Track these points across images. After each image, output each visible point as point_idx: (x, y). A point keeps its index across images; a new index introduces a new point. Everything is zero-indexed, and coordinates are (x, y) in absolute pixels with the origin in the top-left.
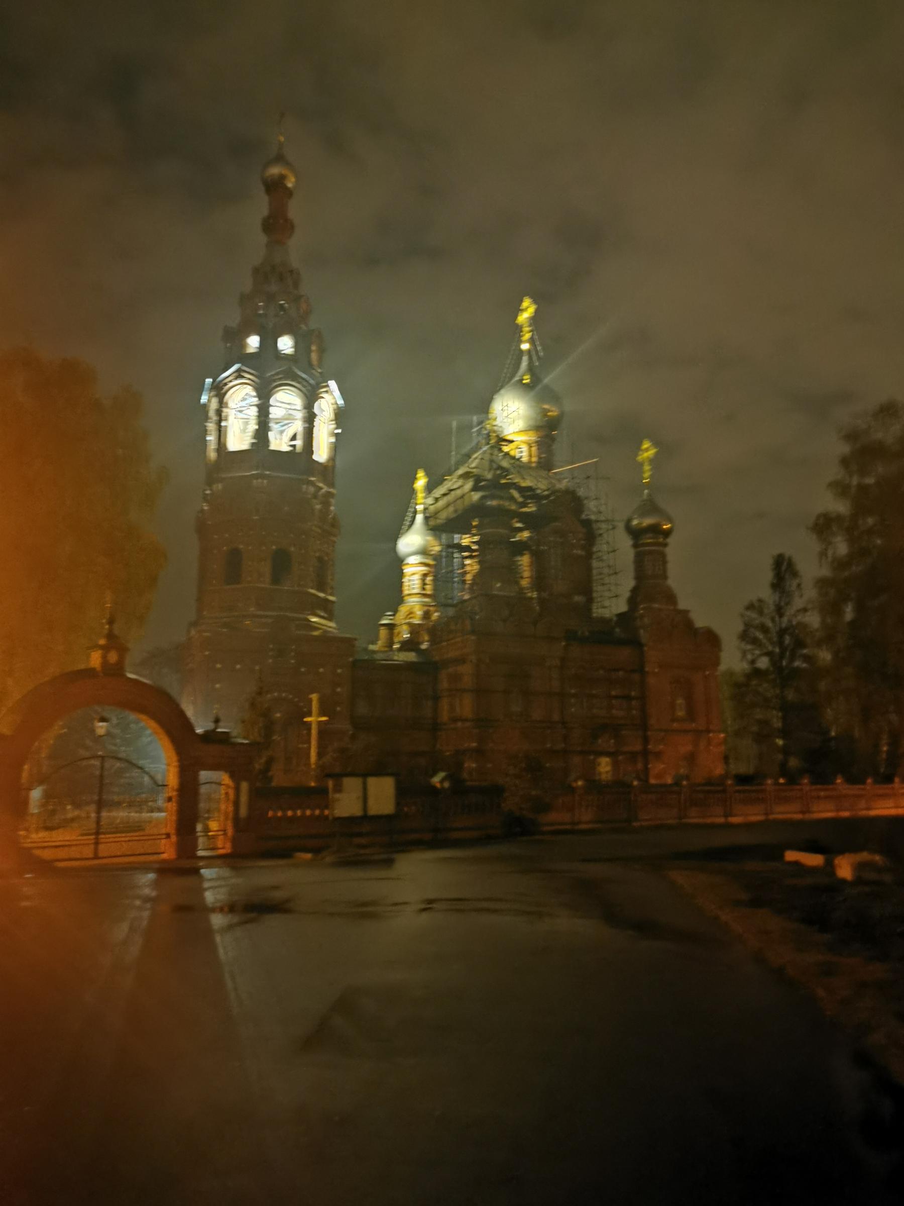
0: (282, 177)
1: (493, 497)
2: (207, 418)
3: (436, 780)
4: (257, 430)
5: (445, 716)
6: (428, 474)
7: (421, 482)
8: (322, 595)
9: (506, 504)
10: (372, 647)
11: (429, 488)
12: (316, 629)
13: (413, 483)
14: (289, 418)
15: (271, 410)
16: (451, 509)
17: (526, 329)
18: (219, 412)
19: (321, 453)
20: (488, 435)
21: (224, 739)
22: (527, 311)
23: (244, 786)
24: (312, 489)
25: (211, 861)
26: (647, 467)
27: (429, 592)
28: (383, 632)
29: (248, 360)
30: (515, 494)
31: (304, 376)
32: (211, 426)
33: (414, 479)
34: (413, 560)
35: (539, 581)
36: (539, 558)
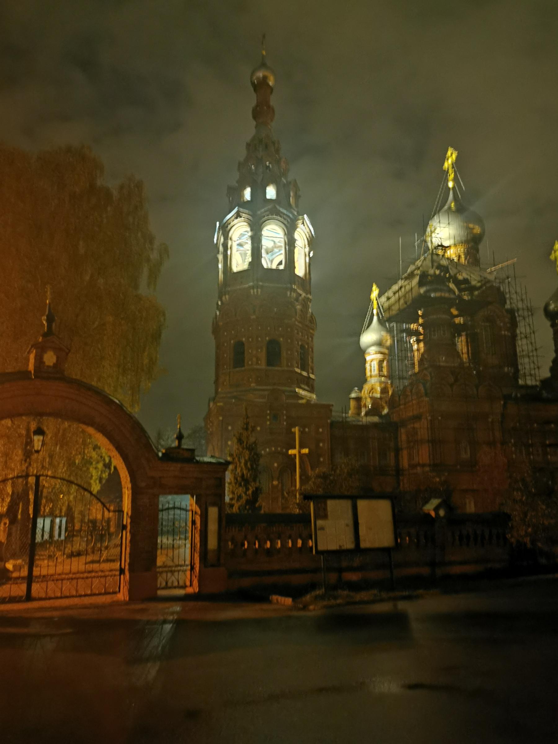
0: (265, 78)
1: (435, 290)
3: (430, 507)
5: (405, 463)
6: (378, 286)
8: (305, 374)
12: (302, 398)
13: (370, 294)
16: (402, 301)
17: (450, 171)
18: (225, 246)
19: (300, 270)
22: (452, 156)
24: (294, 295)
28: (352, 404)
30: (452, 286)
31: (285, 212)
32: (220, 257)
33: (370, 291)
34: (373, 350)
35: (475, 354)
36: (473, 340)
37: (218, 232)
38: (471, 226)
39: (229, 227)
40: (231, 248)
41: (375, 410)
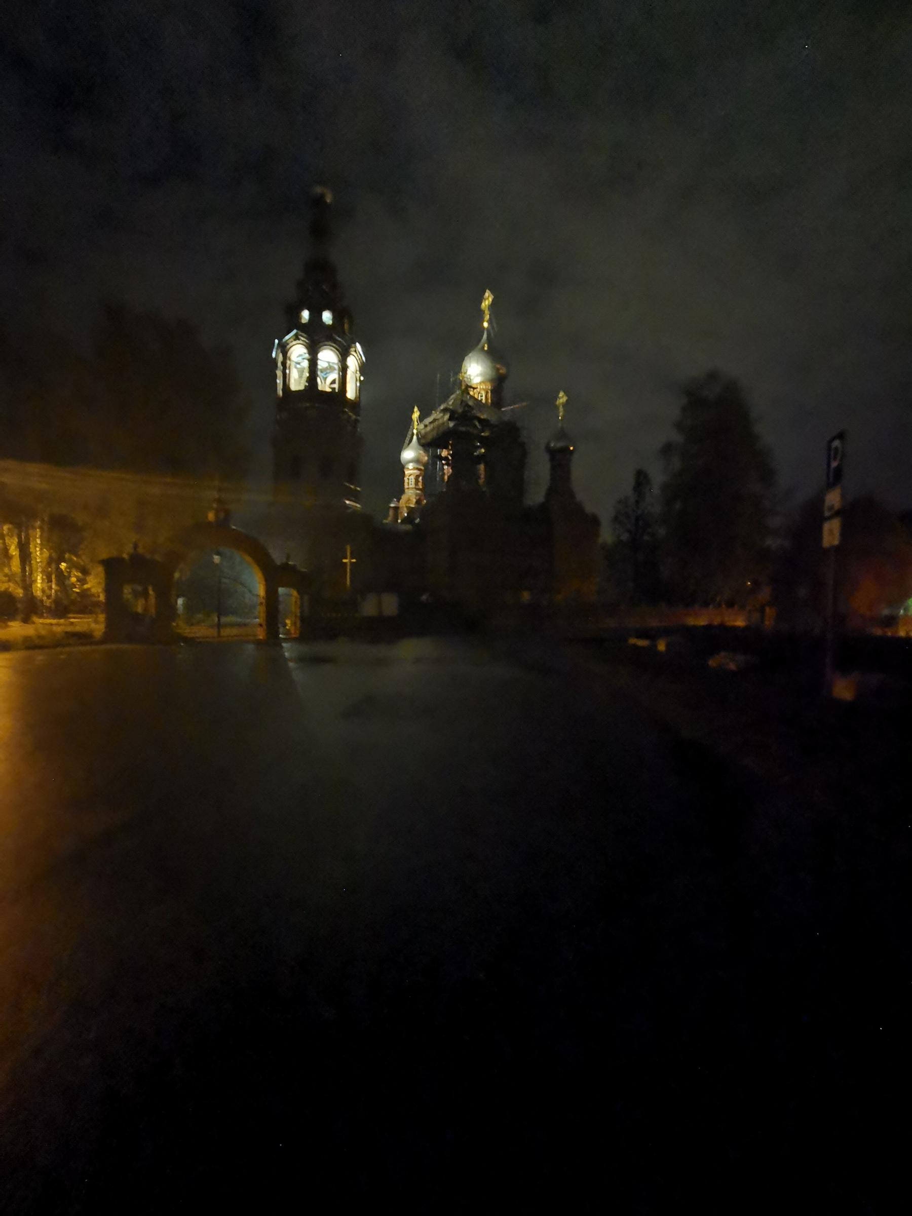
2: (276, 367)
4: (308, 378)
6: (420, 410)
7: (416, 415)
9: (471, 430)
10: (385, 521)
11: (421, 419)
12: (350, 508)
14: (330, 369)
15: (319, 362)
18: (284, 364)
19: (351, 394)
20: (461, 384)
21: (293, 569)
22: (488, 299)
23: (306, 598)
25: (285, 640)
26: (561, 409)
27: (421, 487)
28: (391, 513)
29: (303, 328)
31: (339, 339)
32: (279, 373)
34: (411, 466)
37: (277, 349)
38: (498, 366)
39: (288, 347)
40: (289, 369)
41: (408, 520)
